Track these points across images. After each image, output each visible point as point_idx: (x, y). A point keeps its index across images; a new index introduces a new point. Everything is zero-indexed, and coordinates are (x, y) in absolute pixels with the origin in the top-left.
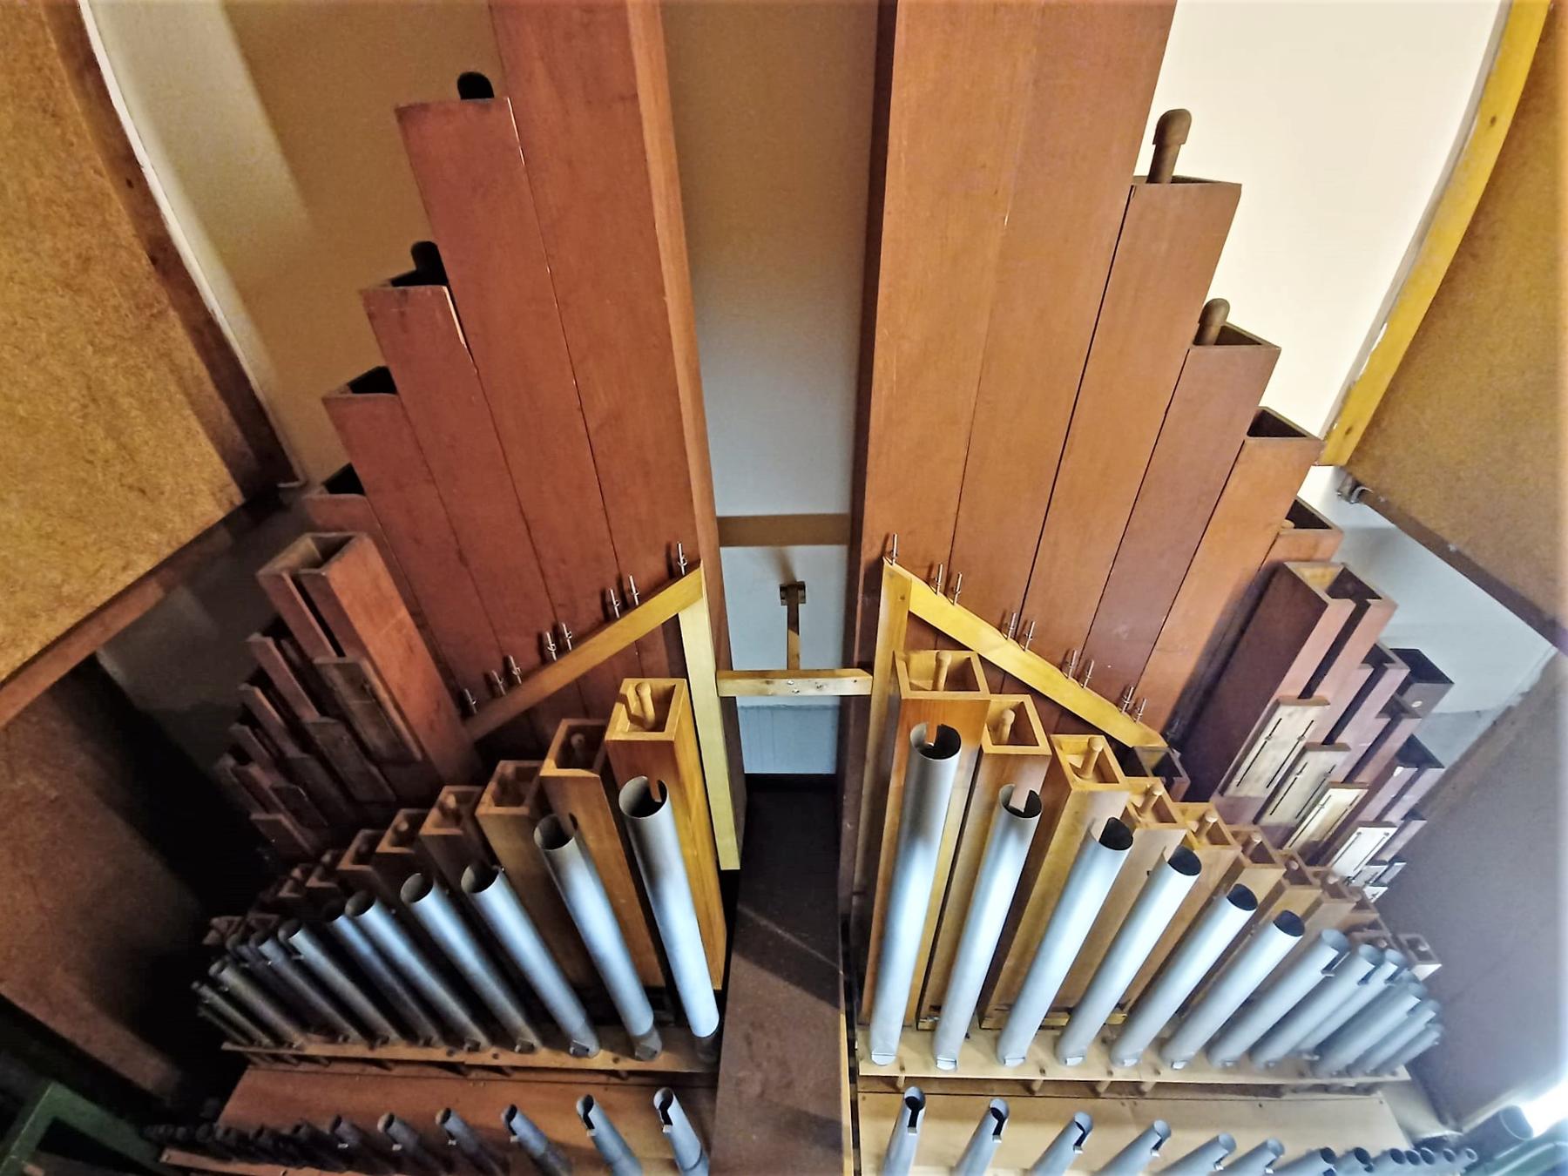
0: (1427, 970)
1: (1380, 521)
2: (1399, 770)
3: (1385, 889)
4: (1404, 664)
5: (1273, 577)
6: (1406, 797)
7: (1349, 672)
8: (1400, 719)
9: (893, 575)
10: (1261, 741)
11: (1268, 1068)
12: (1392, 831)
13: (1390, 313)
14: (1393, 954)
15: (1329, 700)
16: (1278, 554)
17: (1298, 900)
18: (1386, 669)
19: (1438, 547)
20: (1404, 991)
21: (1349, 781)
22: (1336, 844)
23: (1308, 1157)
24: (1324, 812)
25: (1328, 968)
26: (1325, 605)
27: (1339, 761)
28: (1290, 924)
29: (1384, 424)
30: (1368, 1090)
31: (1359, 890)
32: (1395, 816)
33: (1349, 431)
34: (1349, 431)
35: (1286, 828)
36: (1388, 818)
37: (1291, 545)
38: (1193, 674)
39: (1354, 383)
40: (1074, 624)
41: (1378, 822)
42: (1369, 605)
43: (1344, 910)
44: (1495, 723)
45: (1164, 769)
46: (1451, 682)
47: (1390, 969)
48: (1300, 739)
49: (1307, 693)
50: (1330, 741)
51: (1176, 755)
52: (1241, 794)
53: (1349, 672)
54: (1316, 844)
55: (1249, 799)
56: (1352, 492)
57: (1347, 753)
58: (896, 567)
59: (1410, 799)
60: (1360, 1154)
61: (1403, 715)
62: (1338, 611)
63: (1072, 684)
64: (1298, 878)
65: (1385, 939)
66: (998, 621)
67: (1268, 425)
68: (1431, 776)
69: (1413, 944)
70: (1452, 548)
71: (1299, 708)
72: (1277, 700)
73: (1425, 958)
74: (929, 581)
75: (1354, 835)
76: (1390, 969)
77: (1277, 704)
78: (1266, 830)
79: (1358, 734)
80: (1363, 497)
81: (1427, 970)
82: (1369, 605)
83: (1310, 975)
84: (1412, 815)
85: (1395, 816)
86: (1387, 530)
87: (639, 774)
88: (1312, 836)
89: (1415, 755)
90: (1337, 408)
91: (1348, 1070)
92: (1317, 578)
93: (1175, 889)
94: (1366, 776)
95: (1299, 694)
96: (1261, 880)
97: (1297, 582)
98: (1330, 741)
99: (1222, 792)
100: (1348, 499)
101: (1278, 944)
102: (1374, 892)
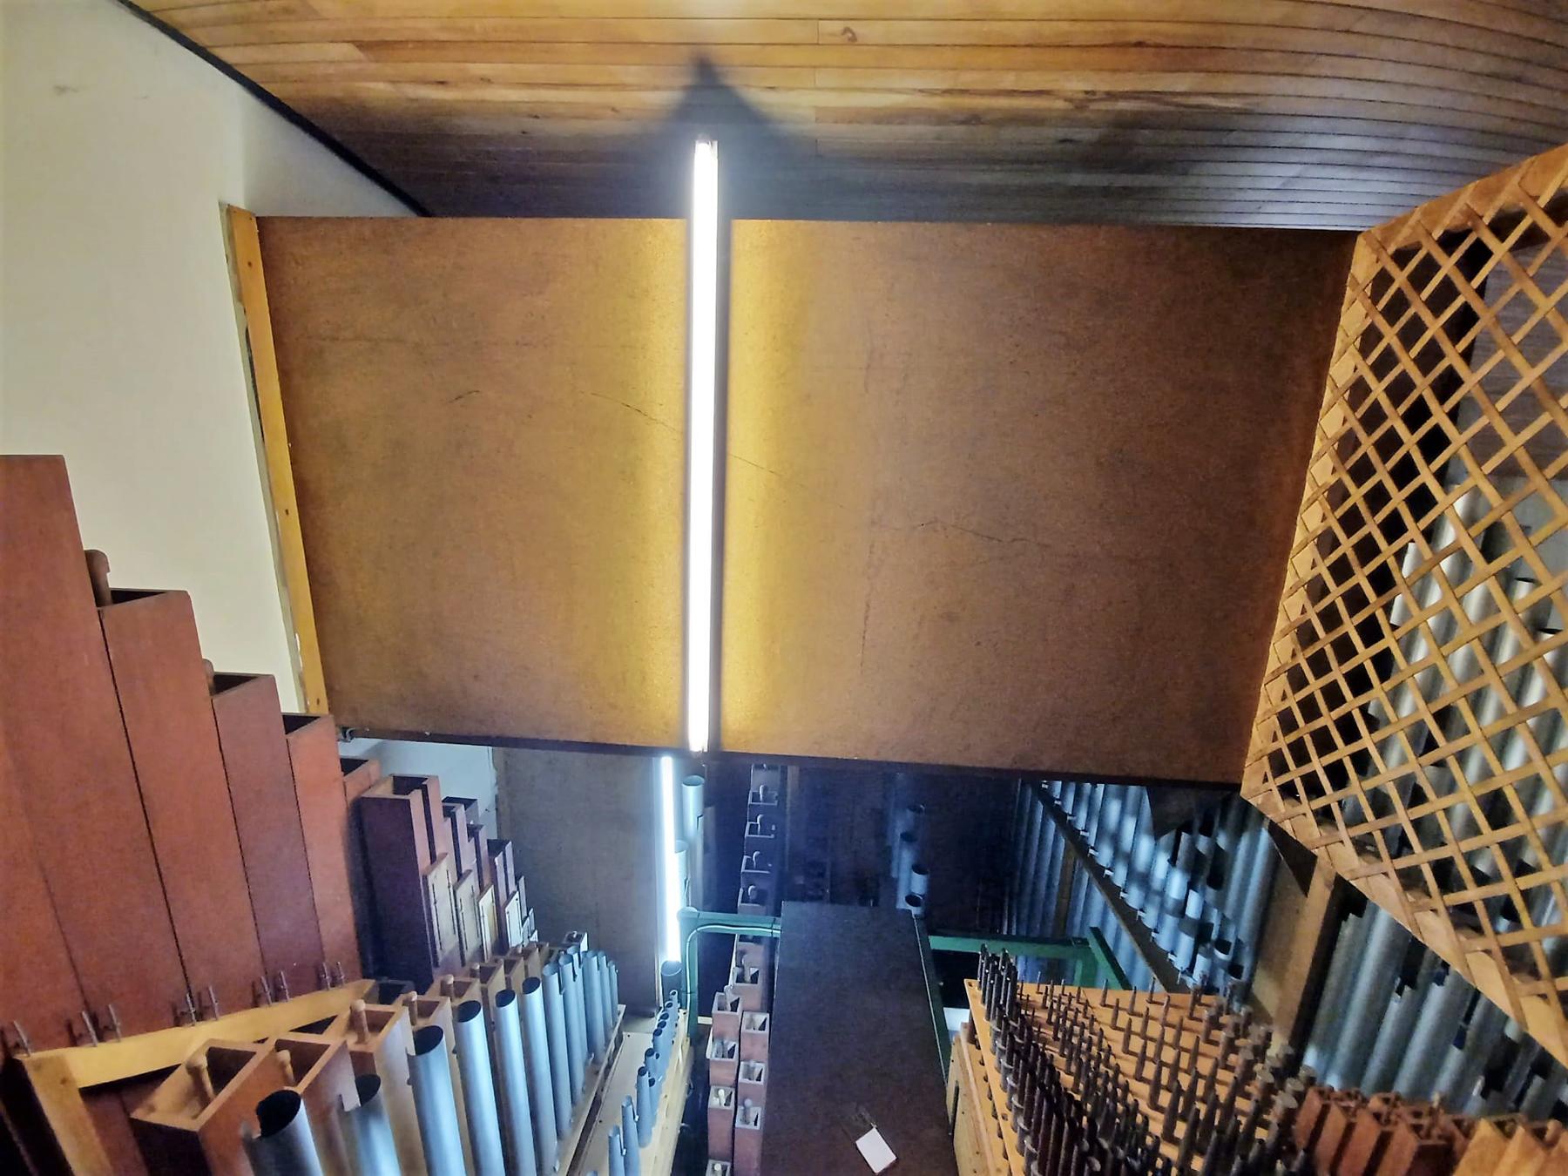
0: (584, 946)
1: (374, 742)
2: (496, 859)
3: (536, 932)
4: (459, 804)
5: (360, 811)
6: (508, 872)
7: (442, 827)
8: (478, 833)
9: (39, 1066)
10: (433, 907)
11: (574, 1125)
12: (517, 895)
13: (294, 626)
14: (570, 951)
15: (445, 851)
16: (352, 795)
17: (518, 975)
18: (454, 813)
19: (419, 737)
20: (589, 960)
21: (482, 890)
22: (504, 931)
23: (639, 1085)
24: (486, 918)
25: (560, 990)
26: (409, 801)
27: (471, 882)
28: (530, 985)
29: (337, 687)
30: (619, 1040)
31: (530, 943)
32: (512, 888)
33: (318, 701)
34: (318, 701)
35: (478, 951)
36: (510, 892)
37: (356, 784)
38: (355, 913)
39: (301, 673)
40: (242, 956)
41: (509, 897)
42: (426, 785)
43: (536, 956)
44: (497, 809)
45: (387, 996)
46: (475, 800)
47: (576, 957)
48: (449, 887)
49: (433, 857)
50: (461, 876)
51: (385, 980)
52: (446, 953)
53: (442, 827)
54: (496, 941)
55: (451, 952)
56: (345, 737)
57: (472, 874)
58: (36, 1055)
59: (511, 870)
60: (649, 1053)
61: (476, 831)
62: (415, 798)
63: (278, 1008)
64: (509, 966)
65: (560, 951)
66: (171, 1019)
67: (293, 723)
68: (509, 848)
69: (571, 939)
70: (428, 733)
71: (436, 869)
72: (423, 877)
73: (579, 938)
74: (74, 1041)
75: (507, 916)
76: (576, 957)
77: (425, 878)
78: (473, 960)
79: (468, 862)
80: (353, 735)
81: (584, 946)
82: (426, 785)
83: (557, 999)
84: (517, 879)
85: (512, 888)
86: (379, 743)
87: (521, 877)
88: (491, 940)
89: (496, 847)
90: (301, 693)
91: (607, 1041)
92: (385, 791)
93: (477, 1025)
94: (486, 881)
95: (430, 861)
96: (498, 983)
97: (380, 802)
98: (461, 876)
99: (436, 965)
100: (346, 741)
101: (536, 996)
102: (535, 937)
